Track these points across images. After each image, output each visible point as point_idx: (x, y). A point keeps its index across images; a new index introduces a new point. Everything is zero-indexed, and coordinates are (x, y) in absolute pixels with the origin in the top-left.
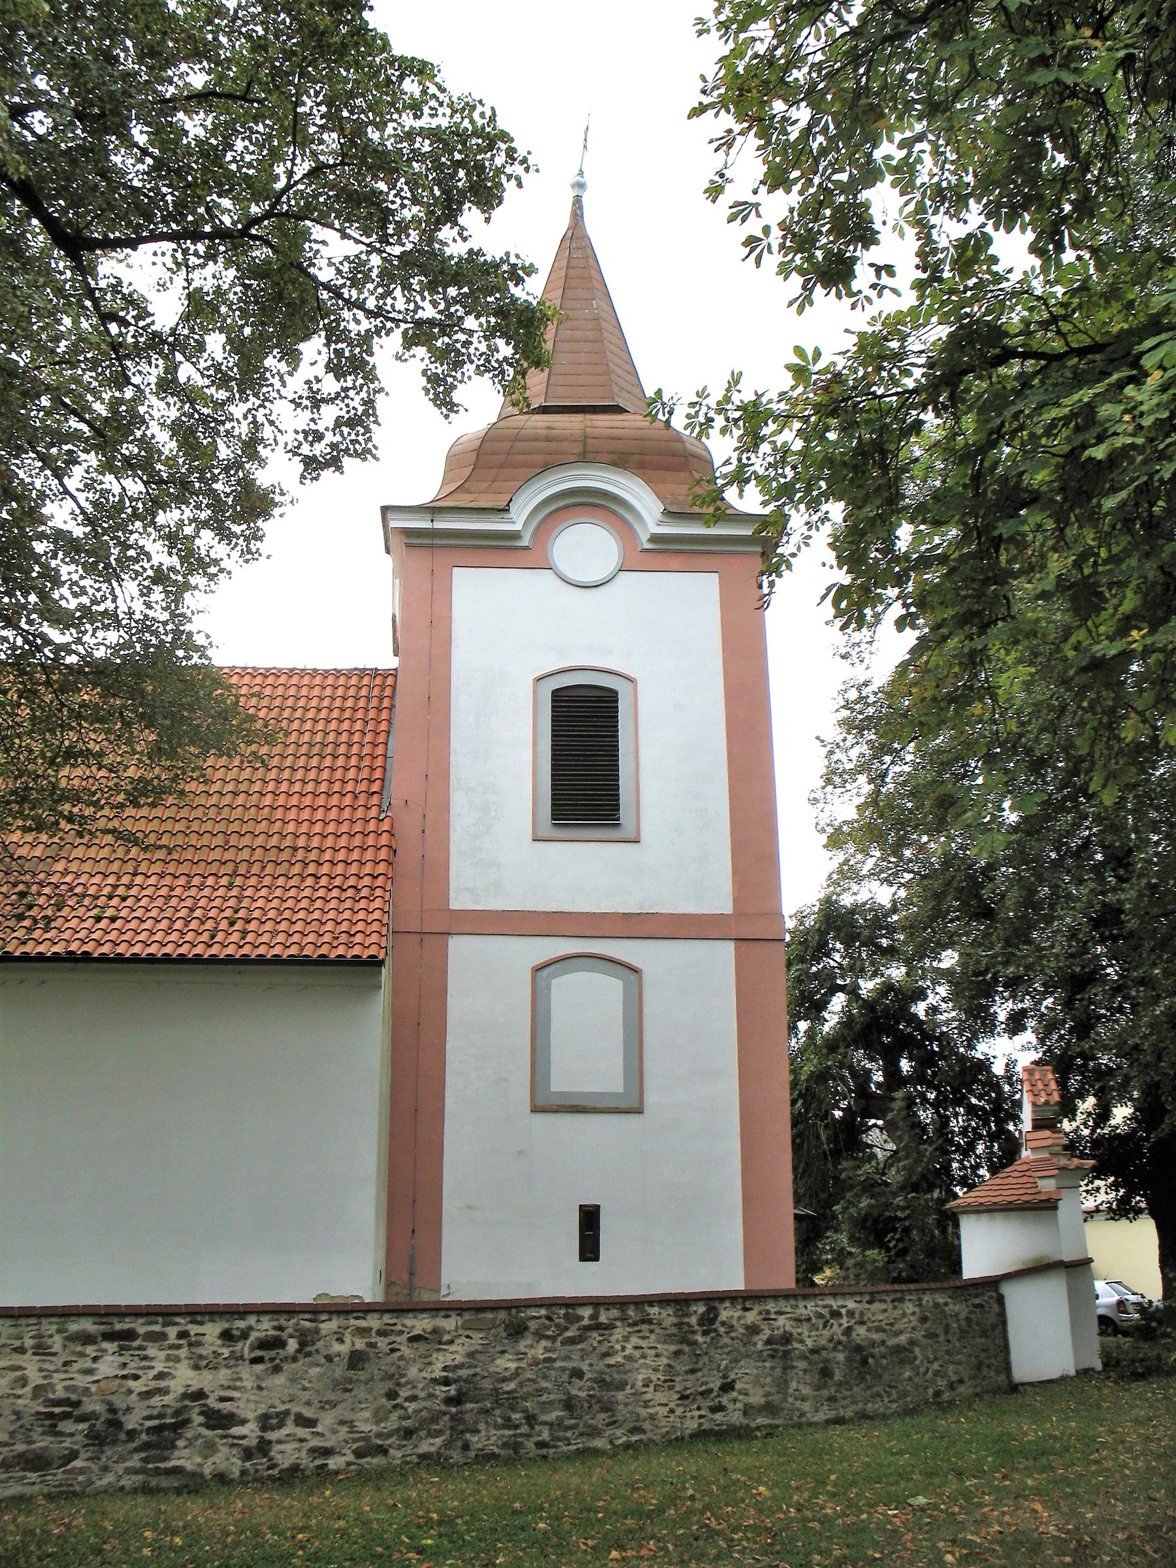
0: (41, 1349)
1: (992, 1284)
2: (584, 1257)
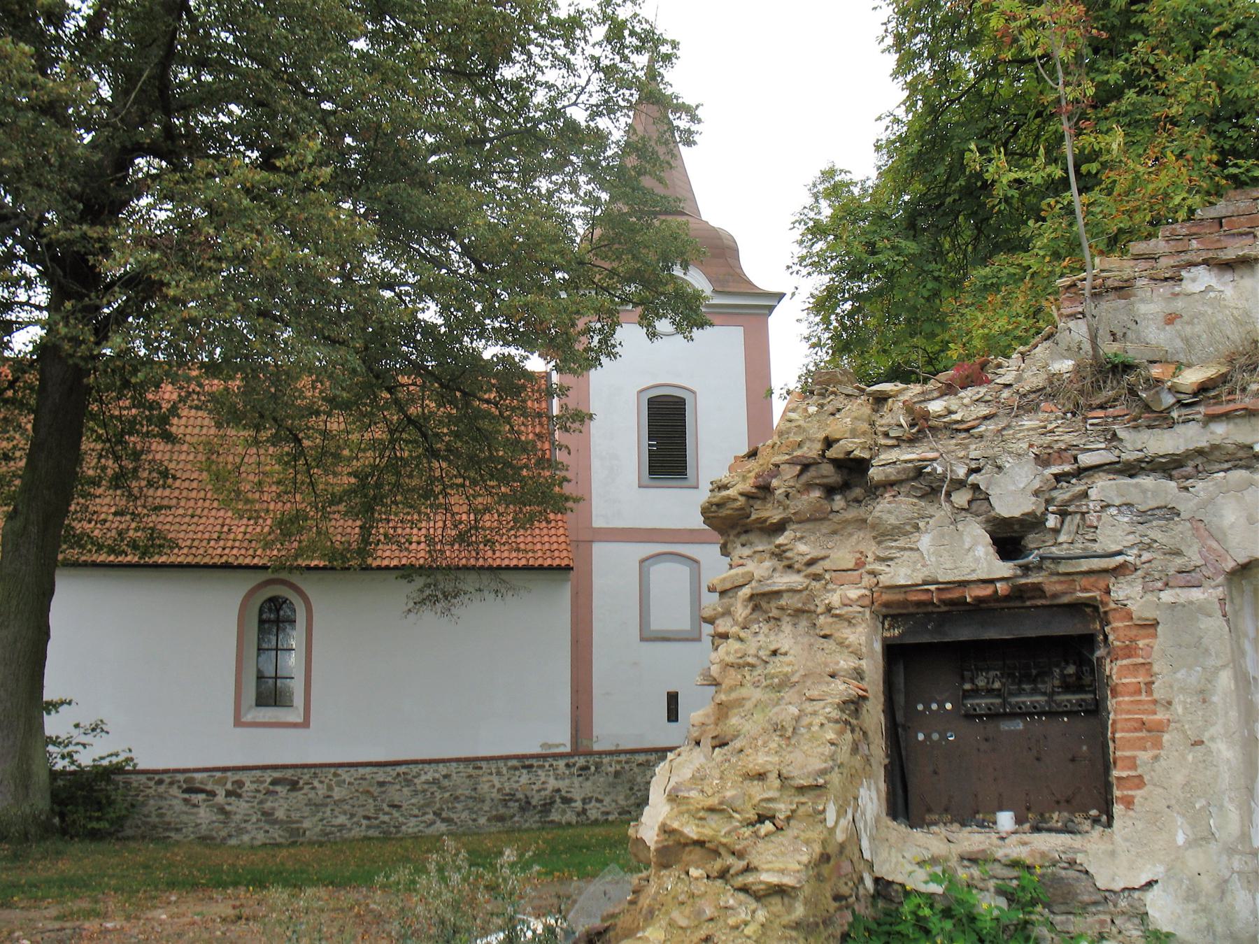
0: (499, 773)
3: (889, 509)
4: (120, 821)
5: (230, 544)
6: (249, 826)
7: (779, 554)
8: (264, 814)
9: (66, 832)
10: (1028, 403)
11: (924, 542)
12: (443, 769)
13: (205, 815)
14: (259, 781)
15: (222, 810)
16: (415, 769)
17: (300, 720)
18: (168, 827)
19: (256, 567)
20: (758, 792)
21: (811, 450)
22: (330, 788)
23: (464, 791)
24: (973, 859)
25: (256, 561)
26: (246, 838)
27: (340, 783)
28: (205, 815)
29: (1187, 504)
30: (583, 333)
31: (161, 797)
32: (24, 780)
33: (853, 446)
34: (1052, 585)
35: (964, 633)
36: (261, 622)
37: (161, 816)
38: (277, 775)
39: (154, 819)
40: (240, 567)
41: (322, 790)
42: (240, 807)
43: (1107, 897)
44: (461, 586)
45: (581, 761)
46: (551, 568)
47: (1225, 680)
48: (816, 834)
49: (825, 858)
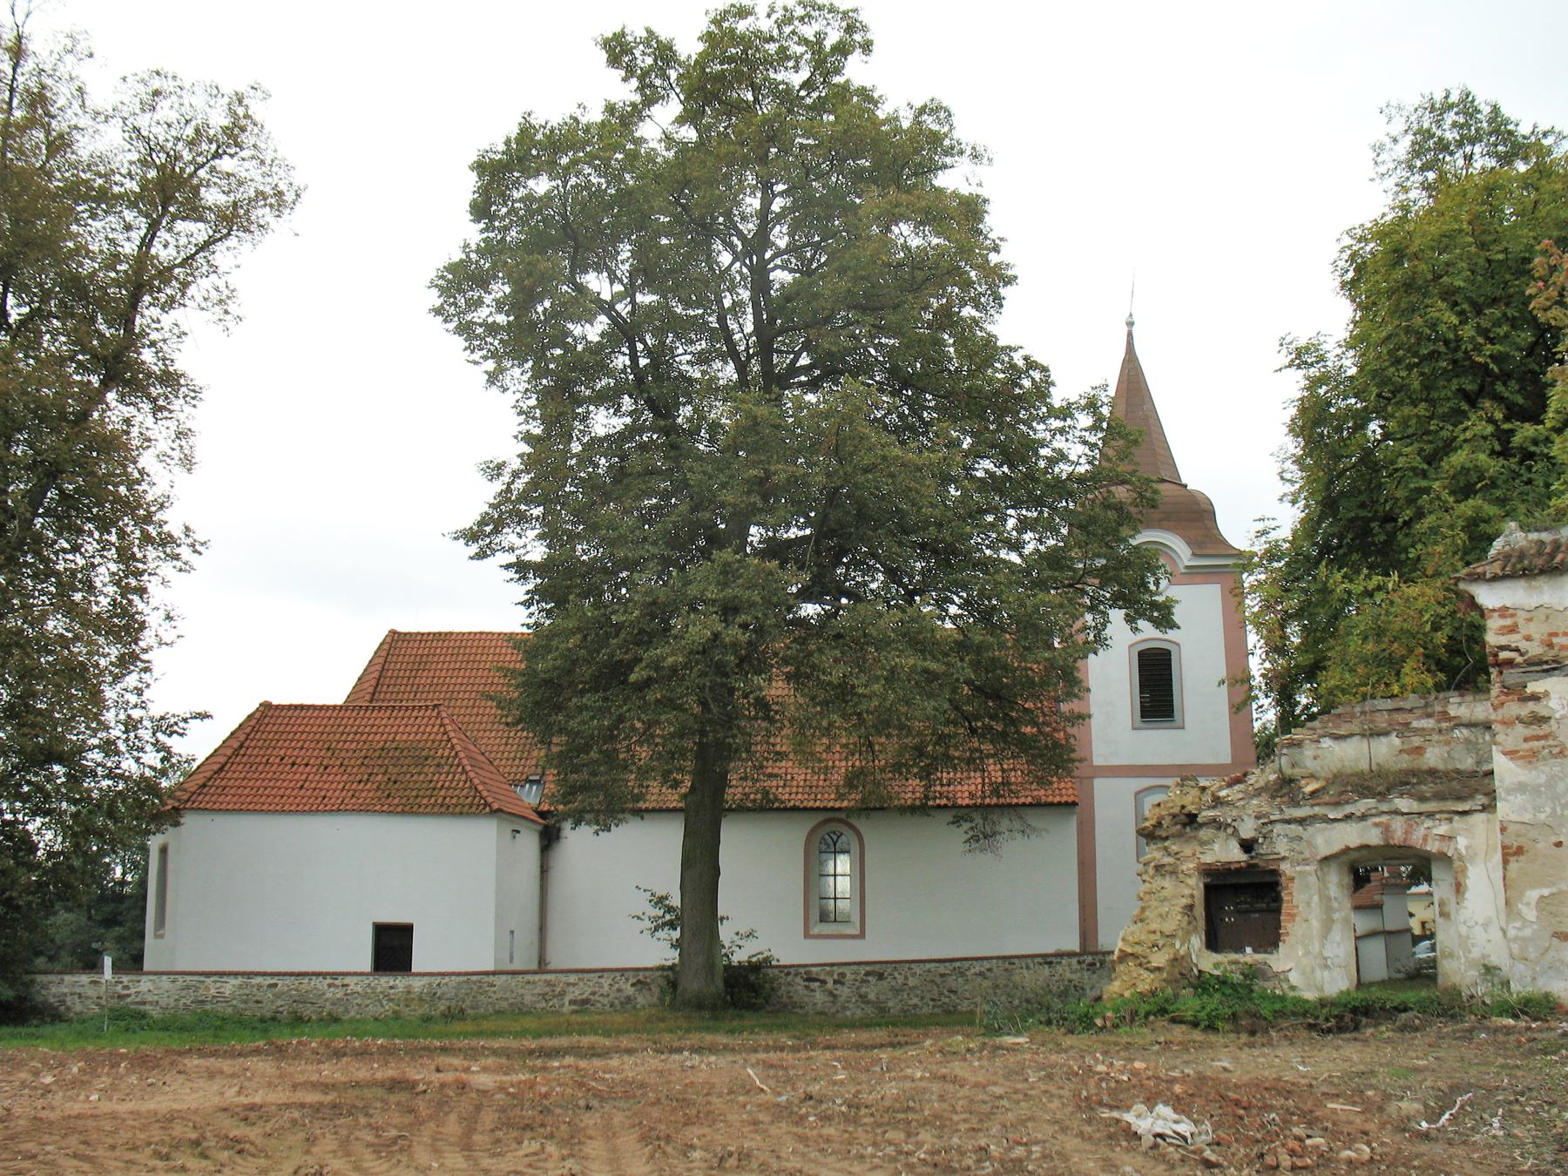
0: (1028, 968)
2: (406, 931)
3: (1204, 834)
7: (1166, 849)
9: (734, 1004)
10: (1258, 793)
11: (1216, 847)
12: (987, 965)
13: (820, 997)
14: (855, 973)
15: (831, 993)
16: (966, 964)
17: (857, 932)
18: (794, 1005)
19: (818, 809)
20: (1153, 937)
21: (1176, 810)
22: (906, 978)
23: (1002, 982)
27: (914, 975)
28: (820, 997)
29: (1305, 835)
30: (1080, 631)
31: (789, 984)
32: (710, 966)
33: (1192, 809)
34: (1262, 864)
35: (1234, 881)
38: (868, 968)
39: (785, 1000)
40: (805, 809)
41: (900, 979)
42: (844, 992)
43: (1277, 975)
44: (997, 828)
45: (1089, 959)
46: (1059, 804)
47: (1316, 898)
48: (1172, 951)
49: (1175, 959)
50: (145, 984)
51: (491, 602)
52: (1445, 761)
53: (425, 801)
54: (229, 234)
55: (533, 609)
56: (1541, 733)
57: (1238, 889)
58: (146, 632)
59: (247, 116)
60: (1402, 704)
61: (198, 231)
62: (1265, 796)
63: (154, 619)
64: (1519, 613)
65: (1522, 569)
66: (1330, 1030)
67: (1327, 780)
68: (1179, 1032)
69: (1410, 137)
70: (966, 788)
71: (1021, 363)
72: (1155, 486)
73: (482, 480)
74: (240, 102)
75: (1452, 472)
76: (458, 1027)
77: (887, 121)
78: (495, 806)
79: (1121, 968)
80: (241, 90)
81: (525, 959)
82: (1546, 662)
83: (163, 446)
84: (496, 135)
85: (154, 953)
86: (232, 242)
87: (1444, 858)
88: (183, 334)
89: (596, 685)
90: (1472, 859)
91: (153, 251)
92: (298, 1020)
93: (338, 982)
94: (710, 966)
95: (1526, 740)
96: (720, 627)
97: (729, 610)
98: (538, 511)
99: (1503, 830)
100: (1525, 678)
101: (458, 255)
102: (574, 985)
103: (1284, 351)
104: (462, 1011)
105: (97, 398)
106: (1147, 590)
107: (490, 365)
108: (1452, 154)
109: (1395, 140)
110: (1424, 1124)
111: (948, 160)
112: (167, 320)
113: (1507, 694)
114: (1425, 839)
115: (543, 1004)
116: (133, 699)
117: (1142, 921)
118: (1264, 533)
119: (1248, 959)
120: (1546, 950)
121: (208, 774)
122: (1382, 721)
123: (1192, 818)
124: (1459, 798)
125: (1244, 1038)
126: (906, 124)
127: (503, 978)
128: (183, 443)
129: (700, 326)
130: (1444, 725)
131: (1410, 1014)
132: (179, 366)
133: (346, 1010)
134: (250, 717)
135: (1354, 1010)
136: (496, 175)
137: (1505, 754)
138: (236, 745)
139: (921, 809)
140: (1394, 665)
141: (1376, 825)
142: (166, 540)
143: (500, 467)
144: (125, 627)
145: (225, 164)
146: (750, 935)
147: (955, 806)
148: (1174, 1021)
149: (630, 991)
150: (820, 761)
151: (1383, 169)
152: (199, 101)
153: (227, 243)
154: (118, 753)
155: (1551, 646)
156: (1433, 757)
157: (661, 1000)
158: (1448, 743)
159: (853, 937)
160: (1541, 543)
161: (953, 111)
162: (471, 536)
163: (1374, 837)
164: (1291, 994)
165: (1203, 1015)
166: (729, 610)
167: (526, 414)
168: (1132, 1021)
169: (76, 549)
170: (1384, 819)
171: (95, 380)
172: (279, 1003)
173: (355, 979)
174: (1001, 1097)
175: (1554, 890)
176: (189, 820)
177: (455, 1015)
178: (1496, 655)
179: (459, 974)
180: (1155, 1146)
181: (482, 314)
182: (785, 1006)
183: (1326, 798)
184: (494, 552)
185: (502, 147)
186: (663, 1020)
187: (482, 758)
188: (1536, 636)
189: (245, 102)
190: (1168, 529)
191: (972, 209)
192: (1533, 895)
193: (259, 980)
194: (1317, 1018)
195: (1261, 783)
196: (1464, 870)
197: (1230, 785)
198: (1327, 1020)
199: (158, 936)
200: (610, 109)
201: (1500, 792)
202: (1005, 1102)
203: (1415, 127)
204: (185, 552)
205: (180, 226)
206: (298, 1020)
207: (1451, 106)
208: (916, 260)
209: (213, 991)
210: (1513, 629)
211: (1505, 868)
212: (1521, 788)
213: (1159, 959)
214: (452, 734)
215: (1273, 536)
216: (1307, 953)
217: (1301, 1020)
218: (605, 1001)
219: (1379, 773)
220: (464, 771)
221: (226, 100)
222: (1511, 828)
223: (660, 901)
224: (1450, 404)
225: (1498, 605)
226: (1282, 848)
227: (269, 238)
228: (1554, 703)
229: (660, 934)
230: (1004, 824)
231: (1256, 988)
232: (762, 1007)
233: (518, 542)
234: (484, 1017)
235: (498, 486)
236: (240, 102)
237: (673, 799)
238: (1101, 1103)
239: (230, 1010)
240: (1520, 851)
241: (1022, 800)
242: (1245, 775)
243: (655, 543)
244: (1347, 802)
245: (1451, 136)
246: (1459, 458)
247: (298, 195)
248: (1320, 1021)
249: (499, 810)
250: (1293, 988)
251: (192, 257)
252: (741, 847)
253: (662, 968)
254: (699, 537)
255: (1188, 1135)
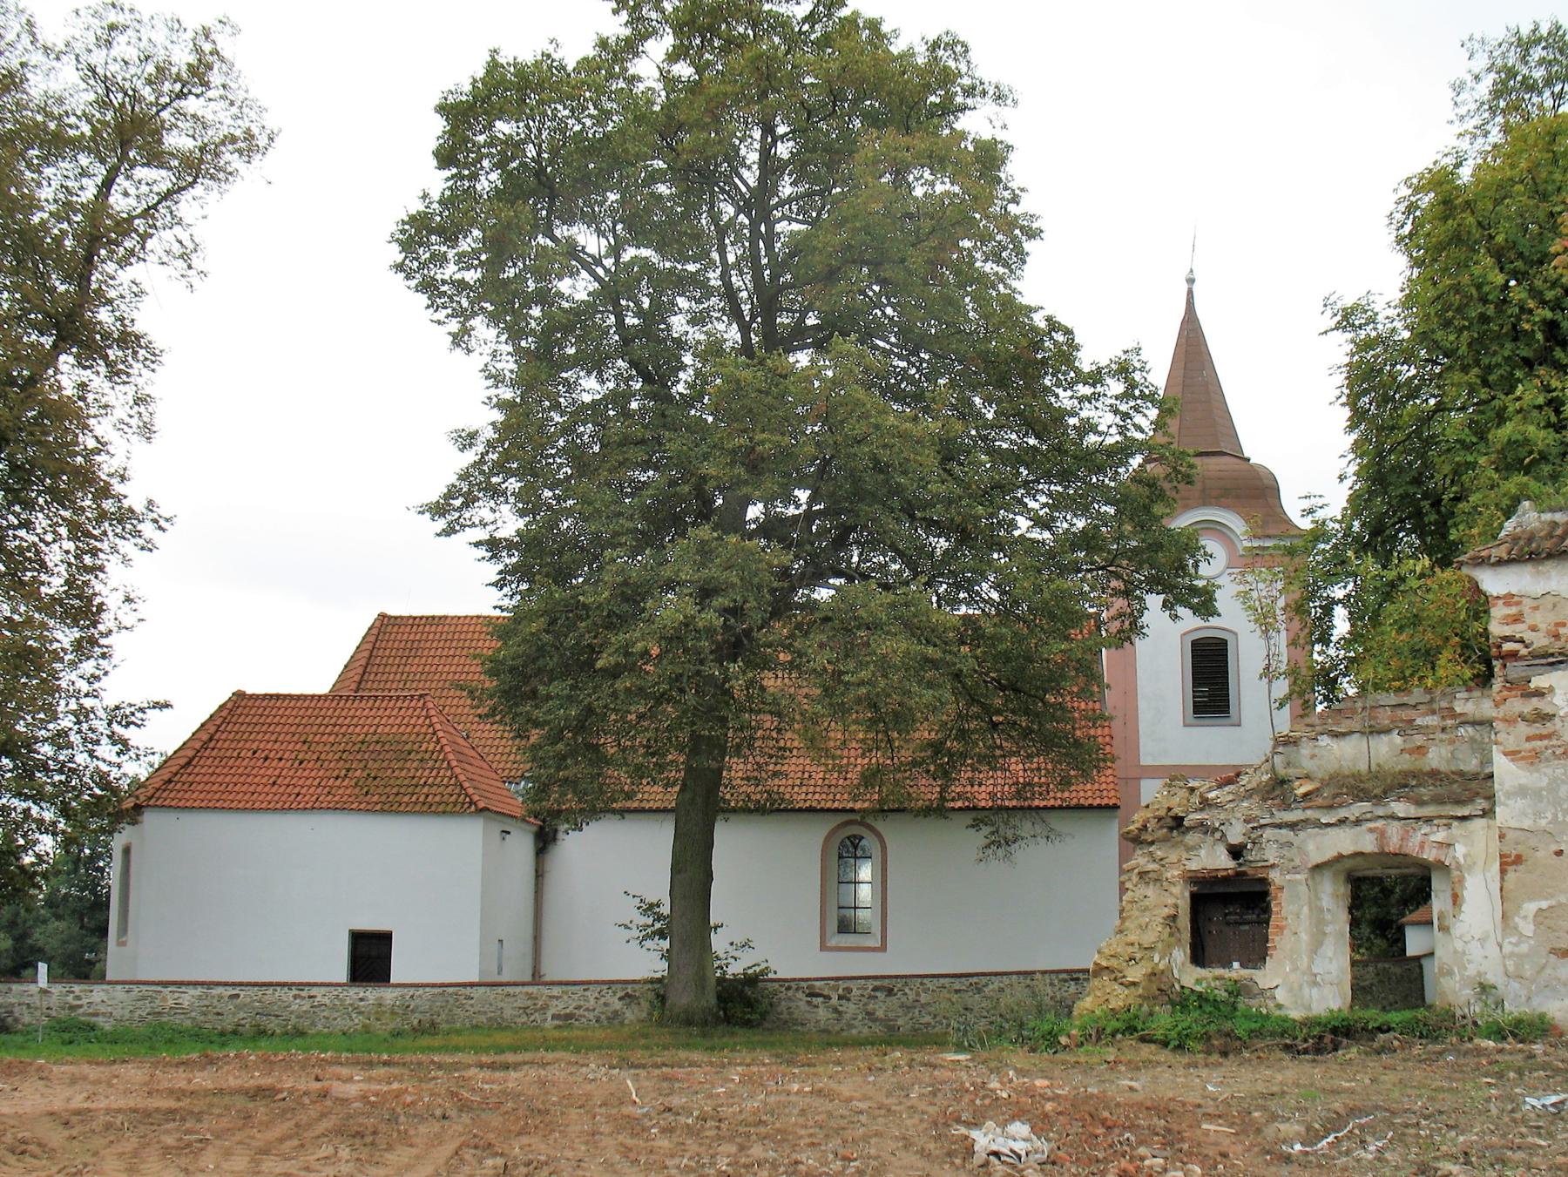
0: (1052, 984)
1: (1417, 959)
2: (385, 939)
3: (1191, 838)
4: (764, 1015)
5: (811, 789)
6: (856, 1023)
8: (868, 1013)
9: (728, 1020)
10: (1250, 794)
11: (1203, 853)
13: (823, 1014)
15: (836, 1010)
16: (984, 980)
19: (836, 810)
20: (1130, 949)
21: (1162, 813)
22: (918, 994)
24: (1216, 978)
25: (836, 805)
26: (854, 1032)
27: (926, 991)
28: (823, 1014)
32: (701, 980)
33: (1178, 811)
34: (1250, 872)
35: (1221, 890)
36: (840, 857)
37: (790, 1014)
38: (877, 983)
39: (785, 1016)
40: (822, 810)
41: (912, 996)
42: (850, 1008)
46: (1099, 807)
47: (1306, 910)
50: (98, 994)
51: (463, 583)
52: (1448, 761)
53: (406, 799)
54: (195, 182)
55: (506, 590)
56: (1545, 732)
57: (1225, 899)
58: (104, 615)
59: (215, 52)
60: (1405, 700)
61: (161, 179)
62: (1256, 798)
63: (113, 601)
64: (1525, 601)
65: (1529, 553)
66: (1306, 1051)
67: (1322, 780)
68: (1147, 1050)
69: (1493, 76)
70: (987, 787)
71: (1043, 325)
72: (1192, 460)
73: (453, 450)
74: (207, 37)
75: (1499, 446)
76: (425, 1041)
77: (902, 56)
78: (481, 805)
79: (1096, 982)
80: (207, 25)
81: (517, 968)
82: (1552, 655)
83: (120, 413)
84: (462, 73)
85: (116, 960)
86: (198, 190)
87: (1441, 866)
88: (145, 292)
89: (565, 671)
90: (1470, 868)
91: (112, 200)
92: (261, 1033)
93: (304, 994)
94: (701, 980)
95: (1528, 739)
96: (692, 610)
97: (705, 593)
98: (513, 484)
99: (1502, 836)
100: (1529, 671)
101: (417, 206)
102: (557, 998)
103: (1329, 313)
104: (433, 1024)
105: (50, 359)
106: (1187, 574)
107: (454, 325)
108: (1540, 94)
109: (1477, 78)
110: (1298, 1147)
111: (969, 101)
112: (125, 276)
113: (1510, 690)
114: (1422, 847)
115: (524, 1019)
116: (84, 686)
117: (1121, 932)
118: (1311, 511)
119: (1234, 975)
120: (1543, 968)
121: (174, 769)
122: (1384, 717)
123: (1178, 821)
124: (1459, 802)
125: (1215, 1057)
126: (921, 60)
127: (482, 989)
128: (142, 409)
129: (697, 281)
130: (1449, 722)
131: (1390, 1035)
132: (138, 328)
133: (313, 1024)
134: (222, 707)
135: (1335, 1031)
136: (463, 115)
137: (1506, 754)
138: (205, 737)
139: (938, 811)
140: (1429, 656)
141: (1371, 830)
142: (125, 517)
143: (473, 436)
144: (82, 609)
145: (191, 105)
146: (746, 945)
147: (975, 808)
148: (1143, 1040)
149: (618, 1005)
150: (834, 758)
151: (1463, 110)
152: (160, 36)
153: (192, 192)
154: (70, 746)
155: (1557, 636)
156: (1437, 757)
157: (650, 1014)
158: (1452, 742)
159: (874, 950)
160: (1555, 524)
161: (971, 45)
162: (437, 510)
163: (1368, 844)
164: (1278, 1013)
165: (1173, 1034)
166: (705, 593)
167: (497, 379)
168: (1099, 1039)
169: (27, 525)
170: (1379, 824)
171: (47, 341)
172: (242, 1015)
173: (323, 990)
174: (861, 1112)
175: (1553, 902)
176: (149, 818)
177: (428, 1029)
178: (1500, 647)
179: (434, 986)
180: (986, 1164)
181: (450, 271)
182: (786, 1022)
183: (1320, 801)
184: (463, 526)
185: (467, 88)
186: (645, 1036)
187: (473, 753)
188: (1543, 626)
189: (213, 36)
190: (1227, 507)
191: (990, 157)
192: (1531, 908)
193: (220, 990)
194: (1295, 1038)
195: (1254, 785)
196: (1461, 880)
197: (1220, 787)
198: (1305, 1041)
199: (121, 944)
200: (603, 44)
201: (1500, 796)
202: (863, 1118)
203: (1499, 62)
204: (147, 529)
205: (140, 172)
206: (261, 1033)
207: (1540, 40)
208: (935, 209)
209: (170, 1002)
210: (1517, 619)
211: (1502, 879)
212: (1522, 791)
213: (1135, 974)
214: (438, 727)
215: (1320, 515)
216: (1295, 969)
217: (1278, 1040)
218: (591, 1015)
219: (1375, 775)
220: (450, 767)
221: (190, 34)
222: (1510, 835)
223: (650, 908)
224: (1501, 372)
225: (1503, 592)
226: (1271, 854)
227: (236, 188)
228: (1558, 699)
229: (648, 944)
230: (1026, 827)
231: (1241, 1006)
232: (759, 1025)
233: (489, 517)
234: (458, 1032)
235: (470, 457)
236: (207, 37)
237: (671, 797)
238: (958, 1121)
239: (188, 1023)
240: (1518, 860)
241: (1052, 802)
242: (1238, 775)
243: (631, 518)
244: (1340, 806)
245: (1539, 74)
246: (1507, 431)
247: (271, 139)
248: (1297, 1042)
249: (486, 809)
250: (1279, 1006)
251: (155, 207)
252: (733, 846)
253: (652, 981)
254: (683, 509)
255: (1023, 1153)
